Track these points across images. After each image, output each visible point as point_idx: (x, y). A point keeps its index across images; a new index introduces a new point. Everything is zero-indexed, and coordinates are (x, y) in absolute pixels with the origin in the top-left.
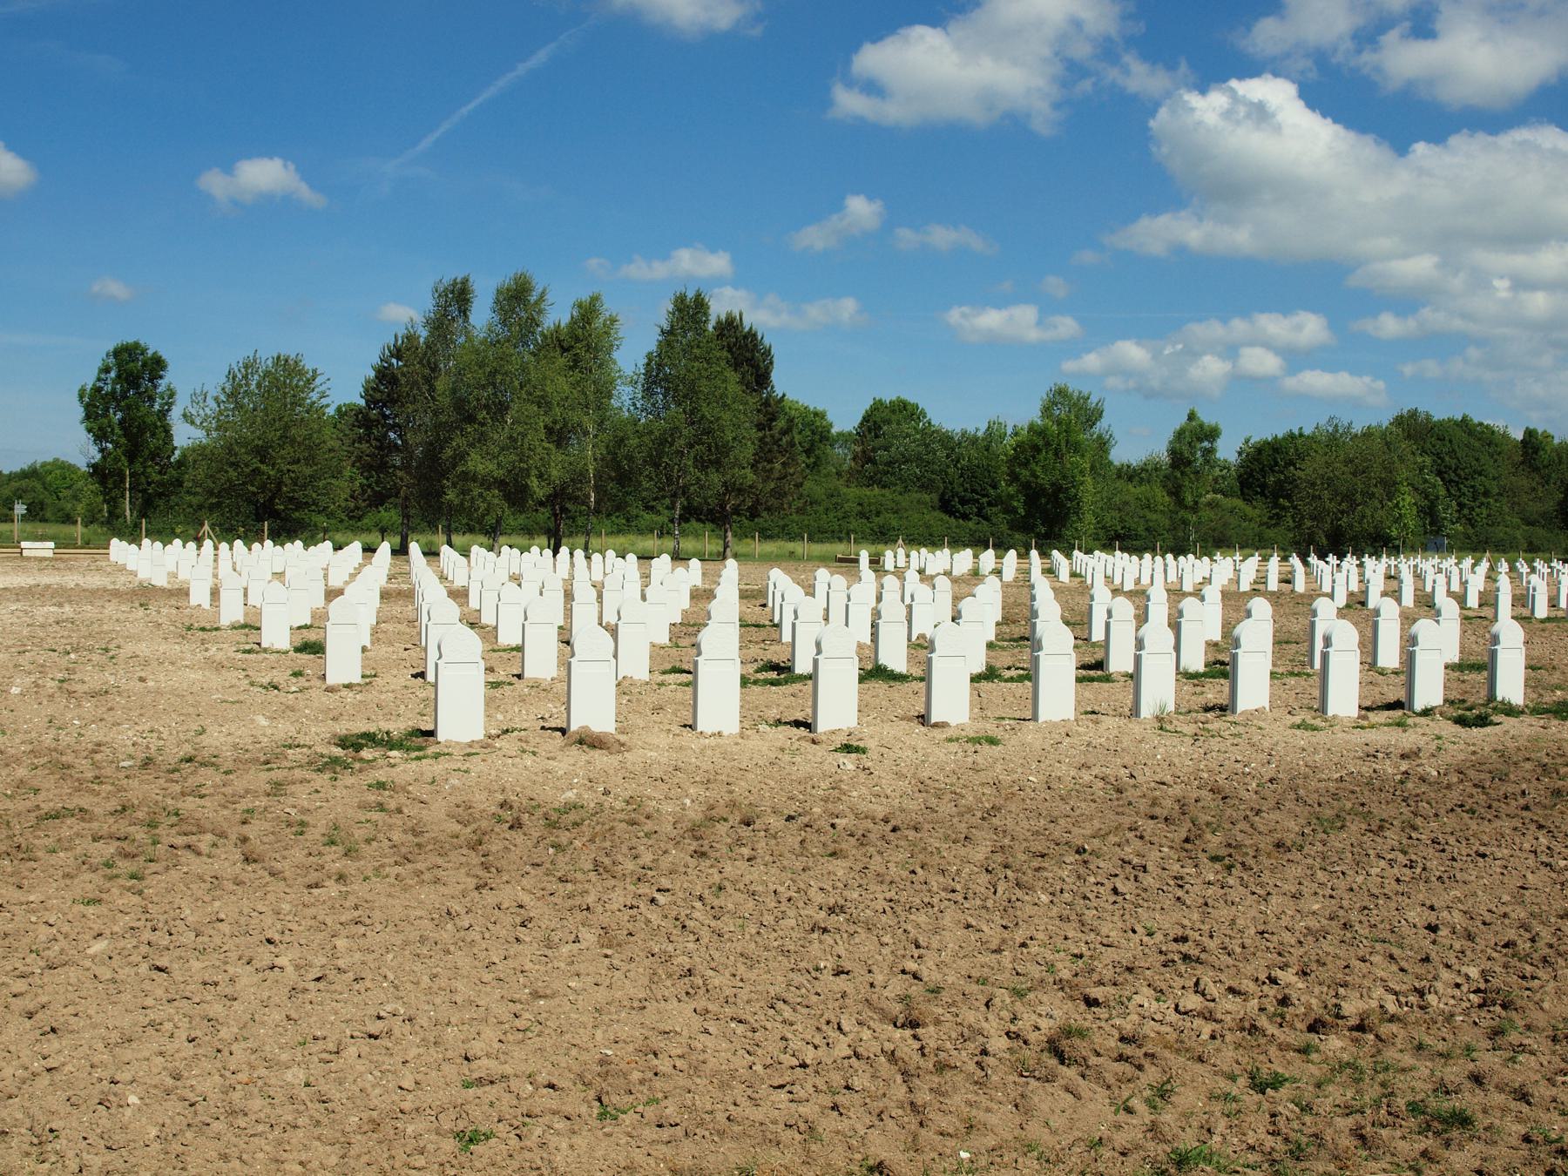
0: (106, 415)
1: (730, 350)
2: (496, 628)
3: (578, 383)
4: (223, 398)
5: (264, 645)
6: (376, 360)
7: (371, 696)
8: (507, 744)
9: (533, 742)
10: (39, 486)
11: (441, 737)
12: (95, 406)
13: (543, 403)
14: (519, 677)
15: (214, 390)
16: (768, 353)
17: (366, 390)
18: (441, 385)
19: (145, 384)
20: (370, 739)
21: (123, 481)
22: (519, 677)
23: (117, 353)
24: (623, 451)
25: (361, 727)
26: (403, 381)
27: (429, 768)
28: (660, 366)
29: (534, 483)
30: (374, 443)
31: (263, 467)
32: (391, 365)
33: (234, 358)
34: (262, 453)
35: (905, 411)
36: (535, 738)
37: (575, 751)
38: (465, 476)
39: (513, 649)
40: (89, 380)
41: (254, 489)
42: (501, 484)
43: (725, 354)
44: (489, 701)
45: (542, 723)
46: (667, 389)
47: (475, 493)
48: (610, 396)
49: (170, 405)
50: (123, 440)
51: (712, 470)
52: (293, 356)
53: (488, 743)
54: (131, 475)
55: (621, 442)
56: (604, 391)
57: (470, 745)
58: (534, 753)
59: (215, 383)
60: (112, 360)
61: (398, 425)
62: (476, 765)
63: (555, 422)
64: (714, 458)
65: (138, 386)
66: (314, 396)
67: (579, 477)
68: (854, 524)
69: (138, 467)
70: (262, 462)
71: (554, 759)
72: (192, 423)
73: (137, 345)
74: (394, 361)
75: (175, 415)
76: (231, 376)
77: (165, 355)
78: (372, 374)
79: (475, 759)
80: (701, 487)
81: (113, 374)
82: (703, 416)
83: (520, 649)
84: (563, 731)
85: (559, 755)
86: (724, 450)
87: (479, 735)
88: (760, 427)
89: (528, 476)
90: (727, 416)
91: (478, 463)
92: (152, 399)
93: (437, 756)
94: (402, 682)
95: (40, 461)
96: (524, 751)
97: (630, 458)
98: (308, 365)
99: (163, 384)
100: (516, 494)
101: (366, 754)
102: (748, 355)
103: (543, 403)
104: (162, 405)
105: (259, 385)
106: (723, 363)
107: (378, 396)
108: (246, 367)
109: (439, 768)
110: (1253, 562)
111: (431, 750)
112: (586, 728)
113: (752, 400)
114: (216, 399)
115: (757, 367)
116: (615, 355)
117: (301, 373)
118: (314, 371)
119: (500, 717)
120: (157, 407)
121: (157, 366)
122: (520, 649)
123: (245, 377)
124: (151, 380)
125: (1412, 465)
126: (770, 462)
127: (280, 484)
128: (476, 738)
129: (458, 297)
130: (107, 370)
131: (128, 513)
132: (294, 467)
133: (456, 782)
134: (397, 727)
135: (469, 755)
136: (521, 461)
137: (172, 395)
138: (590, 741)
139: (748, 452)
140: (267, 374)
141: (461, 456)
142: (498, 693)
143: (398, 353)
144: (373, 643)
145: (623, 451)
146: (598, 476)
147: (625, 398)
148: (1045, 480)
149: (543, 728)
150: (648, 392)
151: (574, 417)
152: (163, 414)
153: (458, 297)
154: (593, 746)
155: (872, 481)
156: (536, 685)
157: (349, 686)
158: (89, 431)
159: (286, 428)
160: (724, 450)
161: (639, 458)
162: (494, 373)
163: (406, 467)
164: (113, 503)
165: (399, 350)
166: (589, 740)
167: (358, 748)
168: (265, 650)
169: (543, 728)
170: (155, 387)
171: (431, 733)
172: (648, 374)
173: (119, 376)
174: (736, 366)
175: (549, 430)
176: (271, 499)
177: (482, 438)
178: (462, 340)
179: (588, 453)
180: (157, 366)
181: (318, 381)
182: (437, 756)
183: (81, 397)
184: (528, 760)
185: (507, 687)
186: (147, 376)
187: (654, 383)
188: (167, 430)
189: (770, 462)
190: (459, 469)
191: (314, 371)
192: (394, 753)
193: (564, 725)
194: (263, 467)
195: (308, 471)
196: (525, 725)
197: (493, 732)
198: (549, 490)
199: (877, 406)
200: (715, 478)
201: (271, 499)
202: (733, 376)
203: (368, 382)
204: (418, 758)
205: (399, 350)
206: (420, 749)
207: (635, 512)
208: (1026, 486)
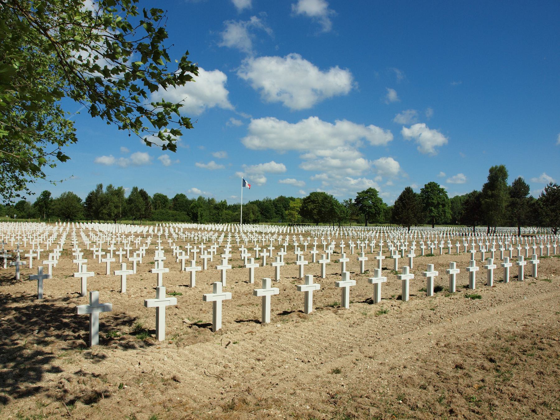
18: (99, 200)
35: (182, 196)
38: (103, 213)
42: (107, 214)
64: (139, 210)
67: (119, 213)
68: (171, 218)
86: (140, 209)
100: (109, 215)
110: (152, 227)
125: (256, 208)
129: (101, 186)
141: (102, 210)
148: (195, 212)
153: (101, 186)
155: (176, 210)
160: (140, 209)
177: (105, 208)
180: (50, 194)
199: (177, 195)
202: (141, 198)
208: (192, 213)
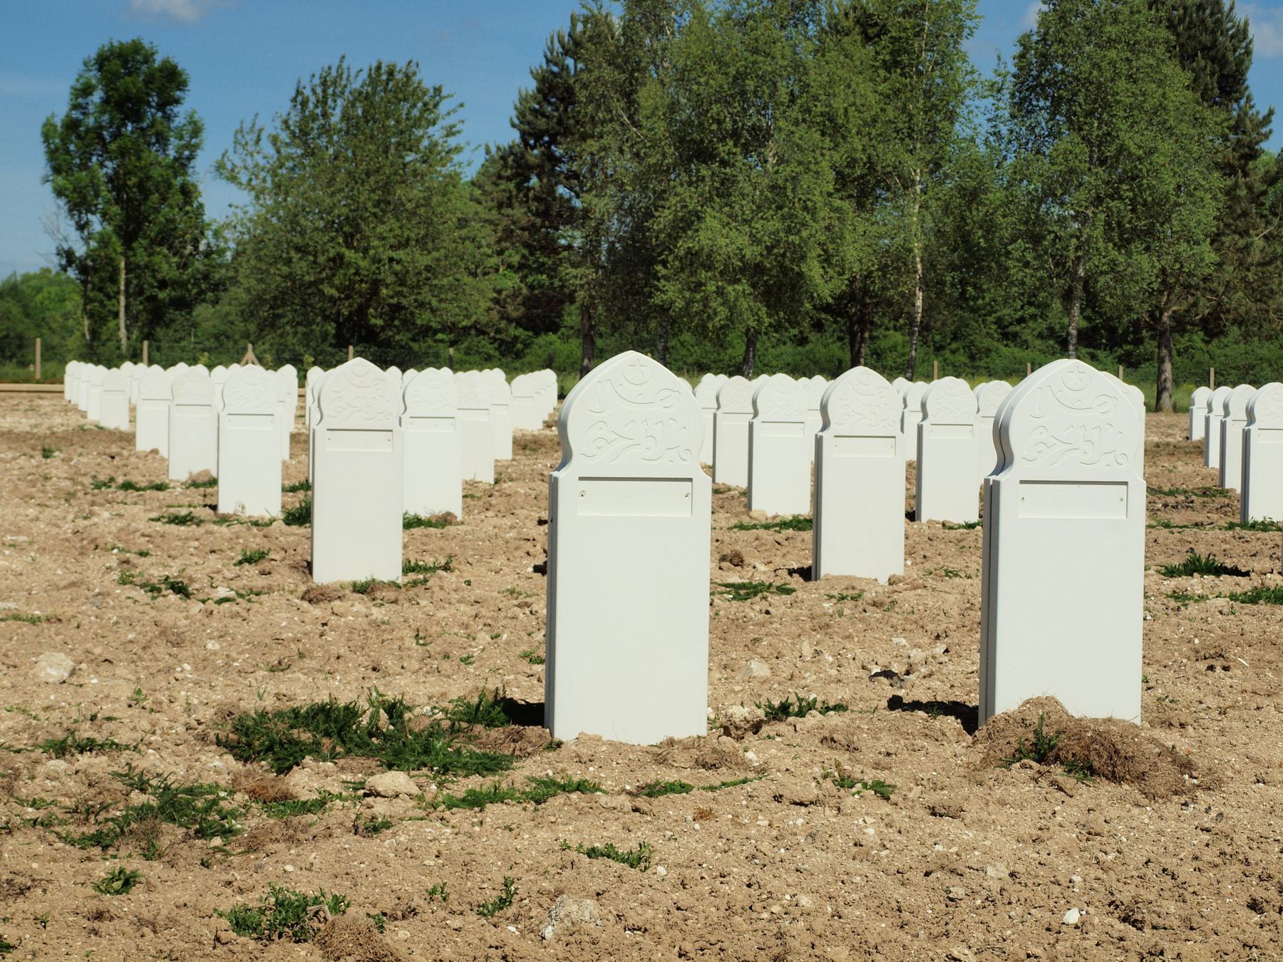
0: (84, 166)
1: (1171, 26)
2: (747, 493)
3: (897, 92)
4: (285, 137)
5: (223, 509)
6: (539, 62)
7: (420, 611)
8: (785, 756)
9: (871, 748)
10: (16, 310)
11: (565, 726)
12: (69, 148)
13: (832, 127)
14: (807, 574)
15: (271, 126)
16: (1242, 34)
17: (521, 115)
18: (648, 96)
19: (151, 113)
20: (334, 726)
21: (114, 280)
22: (807, 574)
23: (102, 61)
24: (978, 214)
25: (304, 690)
26: (582, 96)
27: (507, 840)
28: (1045, 60)
29: (813, 269)
30: (534, 205)
31: (349, 254)
32: (564, 68)
33: (307, 69)
34: (350, 231)
36: (879, 735)
37: (1021, 783)
38: (695, 260)
39: (785, 525)
40: (60, 110)
41: (333, 292)
42: (754, 271)
43: (1164, 33)
44: (721, 630)
45: (887, 690)
46: (1057, 102)
47: (711, 287)
48: (951, 117)
49: (193, 148)
50: (115, 209)
51: (1137, 246)
52: (401, 65)
53: (717, 754)
54: (129, 270)
55: (972, 196)
56: (942, 107)
57: (661, 754)
58: (882, 791)
59: (273, 108)
60: (93, 76)
61: (575, 175)
62: (675, 836)
63: (852, 163)
64: (1142, 221)
65: (137, 117)
66: (436, 132)
69: (141, 257)
70: (349, 245)
71: (954, 813)
72: (233, 178)
73: (136, 48)
74: (570, 62)
75: (202, 173)
76: (299, 100)
77: (183, 63)
78: (531, 85)
79: (669, 806)
80: (1119, 279)
81: (97, 97)
82: (1121, 149)
83: (810, 524)
84: (969, 718)
85: (971, 798)
87: (689, 719)
88: (1228, 169)
89: (803, 258)
90: (1167, 146)
91: (720, 235)
92: (162, 140)
93: (543, 792)
94: (510, 581)
95: (21, 271)
96: (845, 782)
97: (989, 227)
98: (427, 79)
99: (181, 113)
101: (305, 781)
102: (1206, 39)
103: (832, 127)
104: (179, 150)
105: (346, 117)
106: (1160, 50)
107: (542, 123)
108: (324, 83)
109: (569, 825)
111: (524, 772)
112: (1044, 704)
113: (1214, 117)
114: (274, 140)
115: (1223, 62)
116: (966, 45)
117: (418, 93)
118: (438, 90)
119: (760, 669)
120: (172, 153)
121: (170, 81)
122: (810, 524)
123: (323, 102)
124: (161, 107)
126: (1244, 233)
127: (376, 284)
128: (680, 734)
130: (86, 91)
131: (123, 333)
132: (400, 254)
133: (582, 910)
134: (428, 694)
135: (652, 791)
136: (789, 231)
137: (196, 131)
138: (1064, 751)
139: (1203, 214)
140: (360, 96)
142: (752, 610)
143: (574, 47)
144: (467, 509)
145: (978, 214)
146: (930, 265)
147: (979, 119)
149: (895, 703)
150: (1022, 107)
151: (889, 155)
152: (181, 164)
154: (1086, 769)
156: (850, 594)
157: (365, 589)
158: (59, 193)
159: (386, 187)
161: (1006, 225)
162: (739, 77)
163: (589, 253)
164: (99, 319)
165: (577, 44)
166: (1070, 747)
167: (286, 756)
168: (224, 520)
169: (895, 703)
170: (168, 118)
171: (537, 714)
172: (1022, 76)
173: (106, 101)
174: (1186, 58)
175: (842, 179)
176: (362, 311)
177: (724, 189)
178: (687, 18)
179: (909, 223)
180: (170, 81)
181: (444, 107)
182: (543, 792)
183: (47, 137)
184: (866, 817)
185: (775, 599)
186: (154, 100)
187: (1031, 89)
188: (187, 192)
189: (1244, 233)
190: (683, 245)
191: (438, 90)
192: (394, 780)
193: (973, 700)
194: (349, 254)
195: (425, 260)
196: (838, 694)
197: (740, 713)
198: (840, 285)
200: (1145, 264)
201: (362, 311)
202: (1178, 75)
203: (523, 100)
204: (475, 801)
205: (577, 44)
206: (489, 765)
207: (987, 342)
